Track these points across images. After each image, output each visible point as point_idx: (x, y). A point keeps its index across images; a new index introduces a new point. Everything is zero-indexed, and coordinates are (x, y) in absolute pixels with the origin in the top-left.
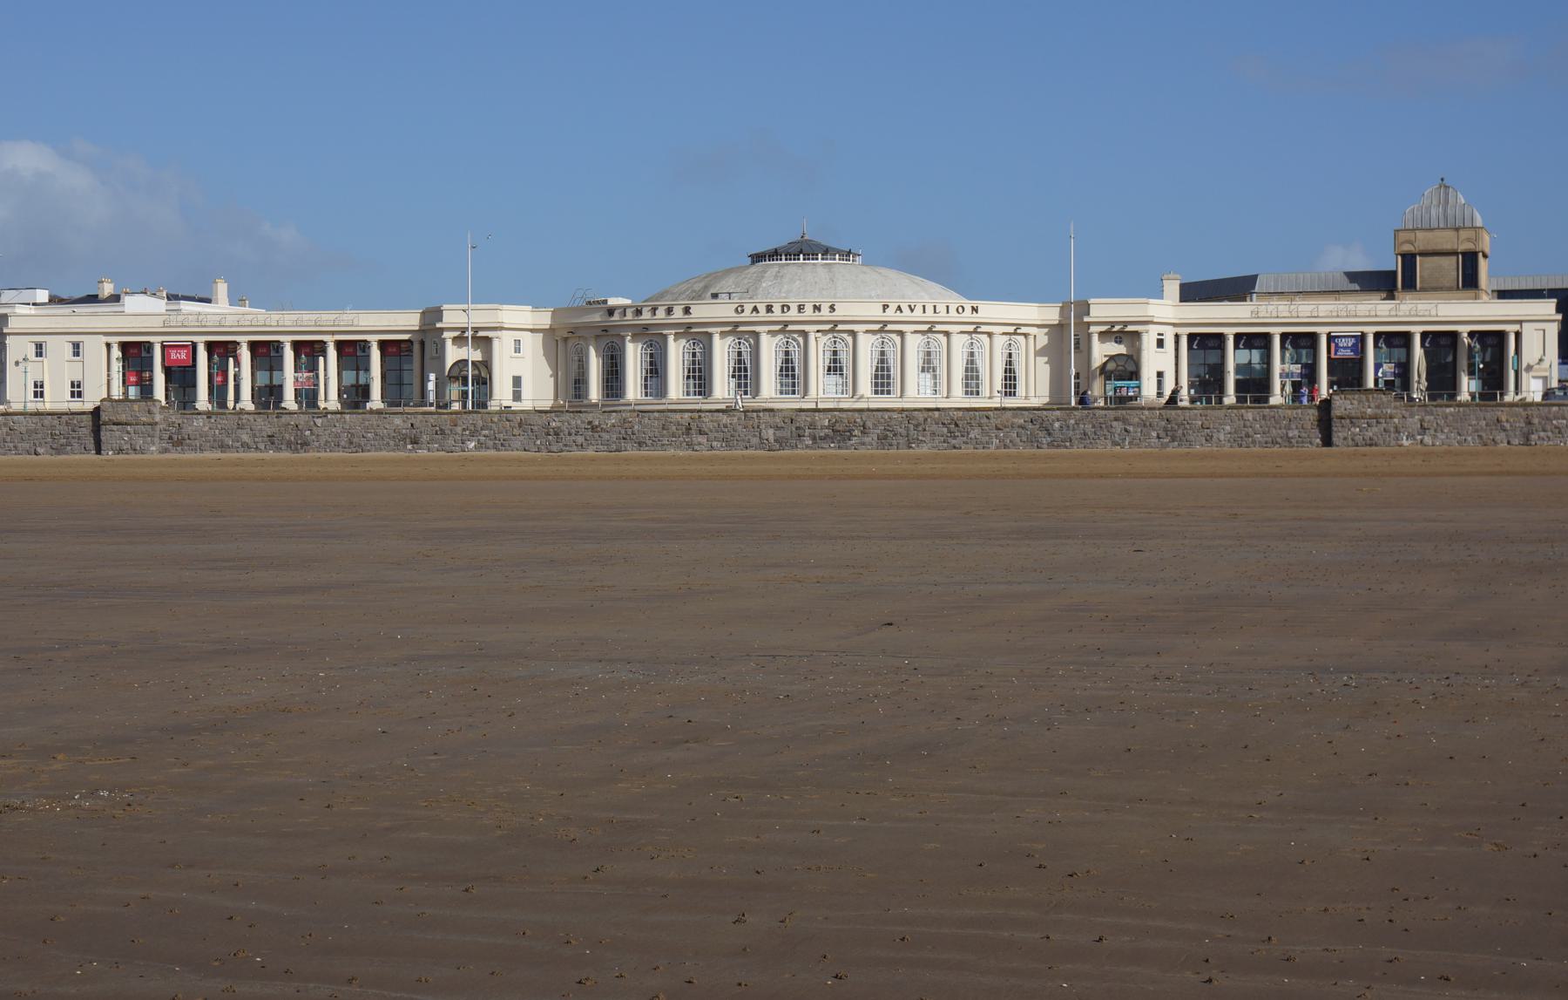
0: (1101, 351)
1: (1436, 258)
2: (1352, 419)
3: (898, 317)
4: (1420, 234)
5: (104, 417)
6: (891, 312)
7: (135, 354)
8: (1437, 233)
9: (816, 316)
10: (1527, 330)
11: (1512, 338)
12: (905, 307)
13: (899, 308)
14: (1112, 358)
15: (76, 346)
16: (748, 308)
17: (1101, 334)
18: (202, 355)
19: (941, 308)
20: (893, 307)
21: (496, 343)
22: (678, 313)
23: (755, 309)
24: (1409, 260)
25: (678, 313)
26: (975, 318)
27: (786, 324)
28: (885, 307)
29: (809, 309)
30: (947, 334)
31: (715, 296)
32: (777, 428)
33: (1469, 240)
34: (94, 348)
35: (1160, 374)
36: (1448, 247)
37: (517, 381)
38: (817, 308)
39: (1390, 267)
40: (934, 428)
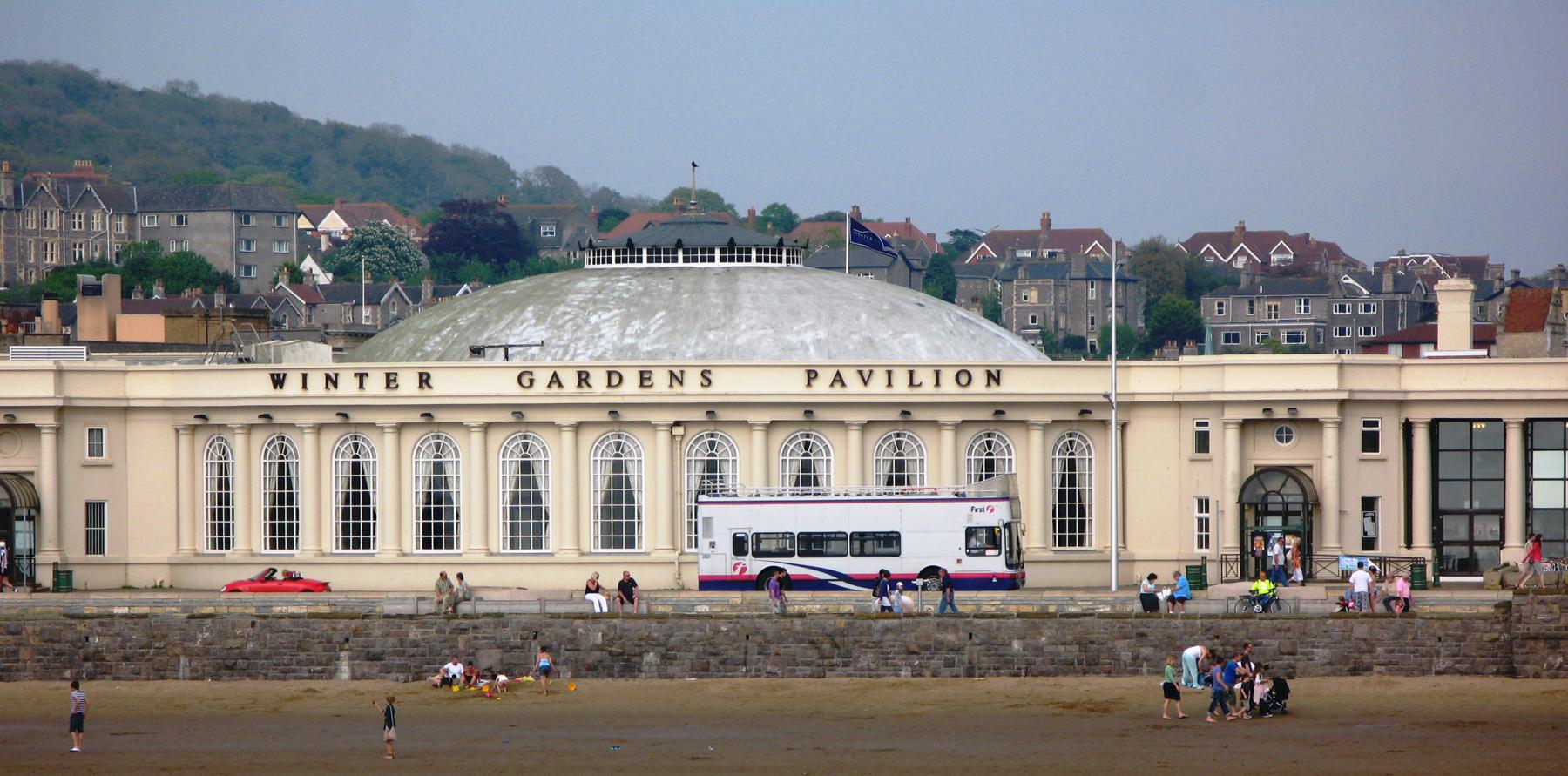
3: (837, 394)
6: (822, 385)
12: (850, 377)
16: (542, 377)
18: (1430, 577)
19: (925, 377)
20: (826, 376)
22: (408, 384)
23: (555, 380)
25: (408, 384)
26: (997, 393)
27: (614, 410)
28: (811, 375)
29: (660, 380)
31: (477, 351)
35: (1369, 504)
37: (95, 511)
38: (676, 378)
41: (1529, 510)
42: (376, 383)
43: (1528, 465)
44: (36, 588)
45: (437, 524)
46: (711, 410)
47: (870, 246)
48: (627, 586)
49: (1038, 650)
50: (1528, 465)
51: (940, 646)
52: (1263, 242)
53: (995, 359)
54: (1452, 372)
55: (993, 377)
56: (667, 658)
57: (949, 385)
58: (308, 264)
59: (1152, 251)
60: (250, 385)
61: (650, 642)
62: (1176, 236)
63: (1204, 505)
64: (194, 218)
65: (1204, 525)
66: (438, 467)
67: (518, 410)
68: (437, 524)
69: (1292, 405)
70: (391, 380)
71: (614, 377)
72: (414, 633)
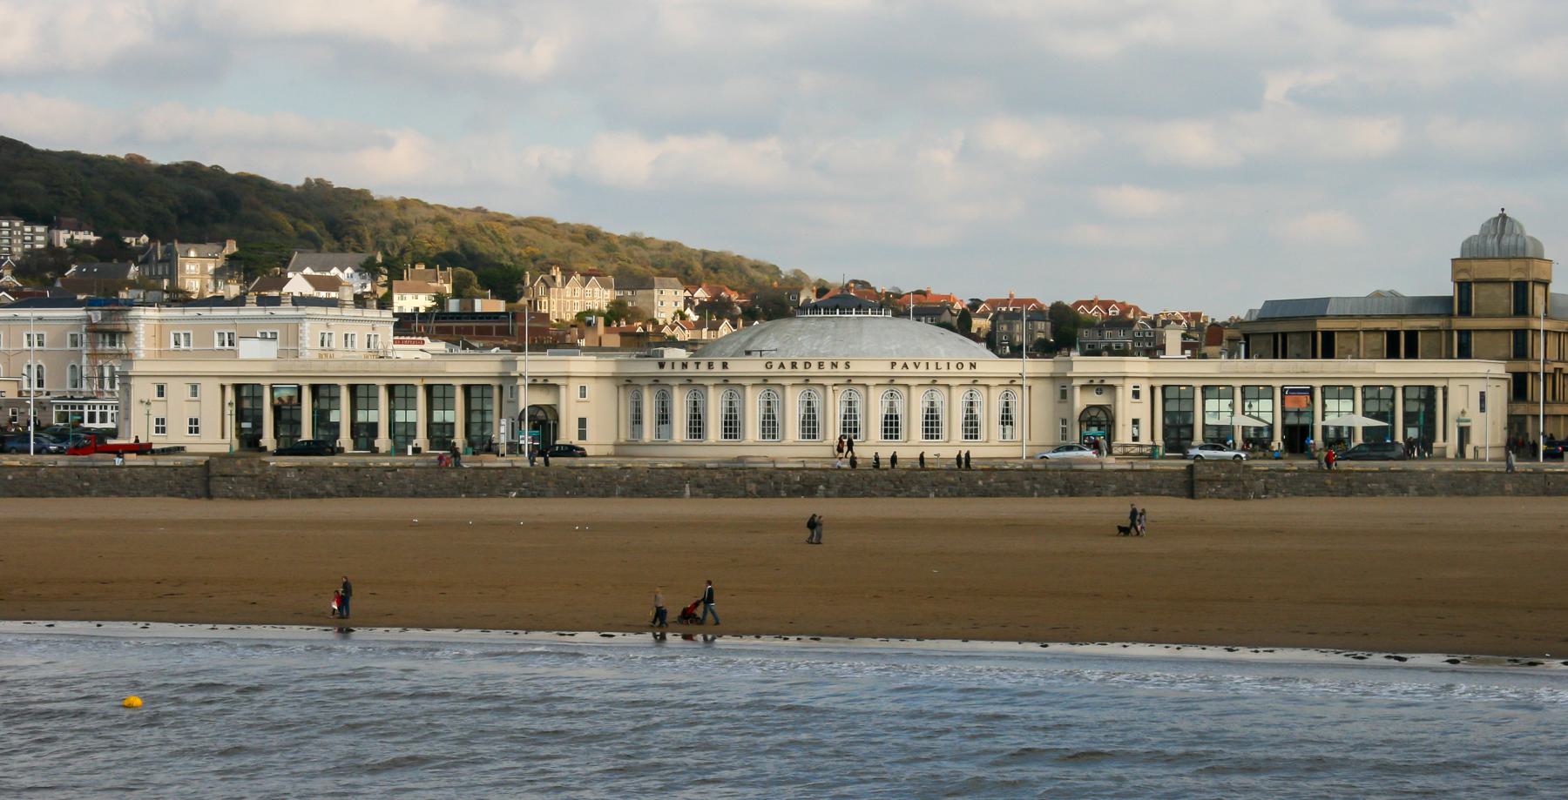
0: (1081, 401)
1: (1490, 287)
2: (1211, 481)
3: (905, 372)
4: (1475, 264)
5: (213, 471)
6: (898, 369)
7: (245, 399)
8: (1492, 263)
9: (834, 372)
10: (1454, 388)
11: (1440, 394)
12: (910, 365)
13: (905, 366)
14: (1090, 407)
15: (194, 387)
16: (776, 365)
17: (1082, 387)
19: (943, 365)
20: (900, 365)
21: (563, 390)
22: (718, 368)
23: (782, 366)
24: (1464, 287)
25: (718, 368)
26: (725, 373)
28: (893, 364)
29: (827, 365)
30: (908, 386)
31: (748, 353)
32: (758, 482)
33: (1519, 269)
34: (210, 390)
35: (1135, 422)
36: (1500, 276)
38: (834, 365)
39: (1451, 294)
40: (884, 483)
41: (1204, 425)
42: (703, 368)
43: (1324, 406)
44: (375, 451)
45: (732, 427)
46: (849, 379)
47: (930, 310)
48: (894, 459)
49: (990, 485)
50: (1324, 406)
51: (946, 483)
52: (1106, 305)
53: (973, 359)
54: (1176, 365)
55: (973, 366)
56: (828, 487)
57: (953, 368)
58: (688, 311)
59: (1058, 308)
60: (650, 368)
61: (821, 481)
62: (1069, 301)
63: (1064, 421)
64: (639, 292)
65: (1064, 430)
66: (891, 404)
67: (765, 379)
68: (732, 427)
69: (546, 378)
70: (710, 365)
71: (807, 364)
72: (718, 476)
